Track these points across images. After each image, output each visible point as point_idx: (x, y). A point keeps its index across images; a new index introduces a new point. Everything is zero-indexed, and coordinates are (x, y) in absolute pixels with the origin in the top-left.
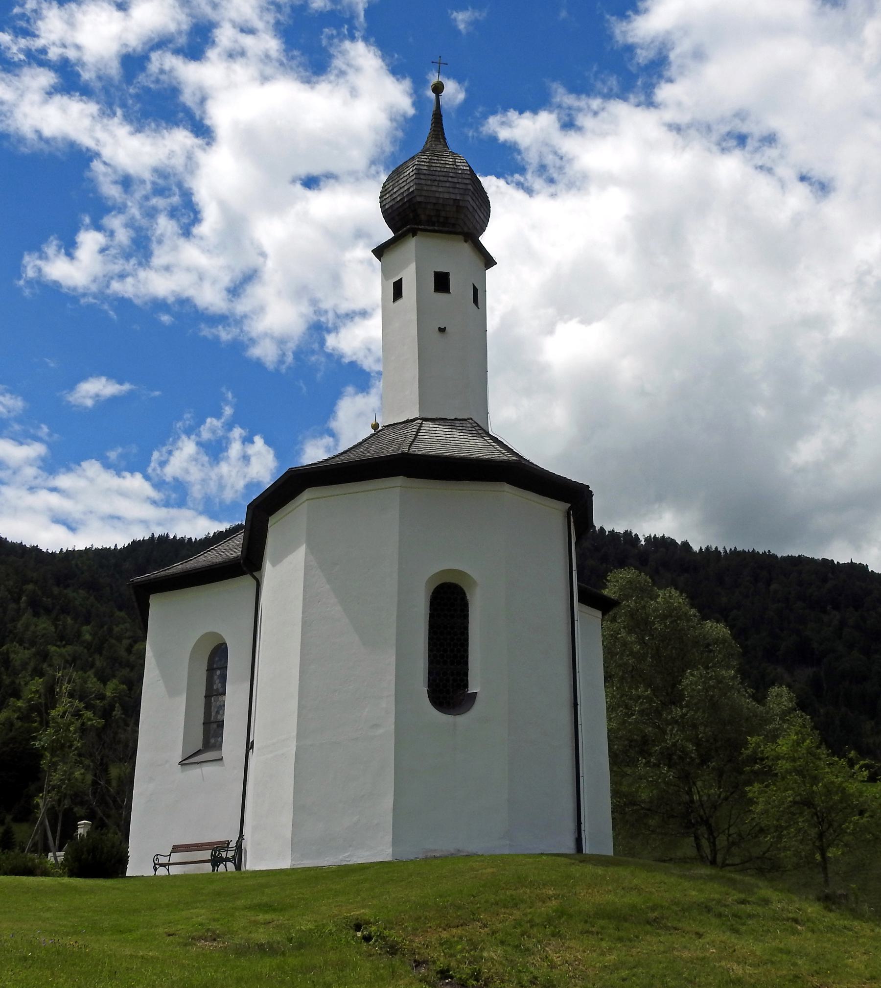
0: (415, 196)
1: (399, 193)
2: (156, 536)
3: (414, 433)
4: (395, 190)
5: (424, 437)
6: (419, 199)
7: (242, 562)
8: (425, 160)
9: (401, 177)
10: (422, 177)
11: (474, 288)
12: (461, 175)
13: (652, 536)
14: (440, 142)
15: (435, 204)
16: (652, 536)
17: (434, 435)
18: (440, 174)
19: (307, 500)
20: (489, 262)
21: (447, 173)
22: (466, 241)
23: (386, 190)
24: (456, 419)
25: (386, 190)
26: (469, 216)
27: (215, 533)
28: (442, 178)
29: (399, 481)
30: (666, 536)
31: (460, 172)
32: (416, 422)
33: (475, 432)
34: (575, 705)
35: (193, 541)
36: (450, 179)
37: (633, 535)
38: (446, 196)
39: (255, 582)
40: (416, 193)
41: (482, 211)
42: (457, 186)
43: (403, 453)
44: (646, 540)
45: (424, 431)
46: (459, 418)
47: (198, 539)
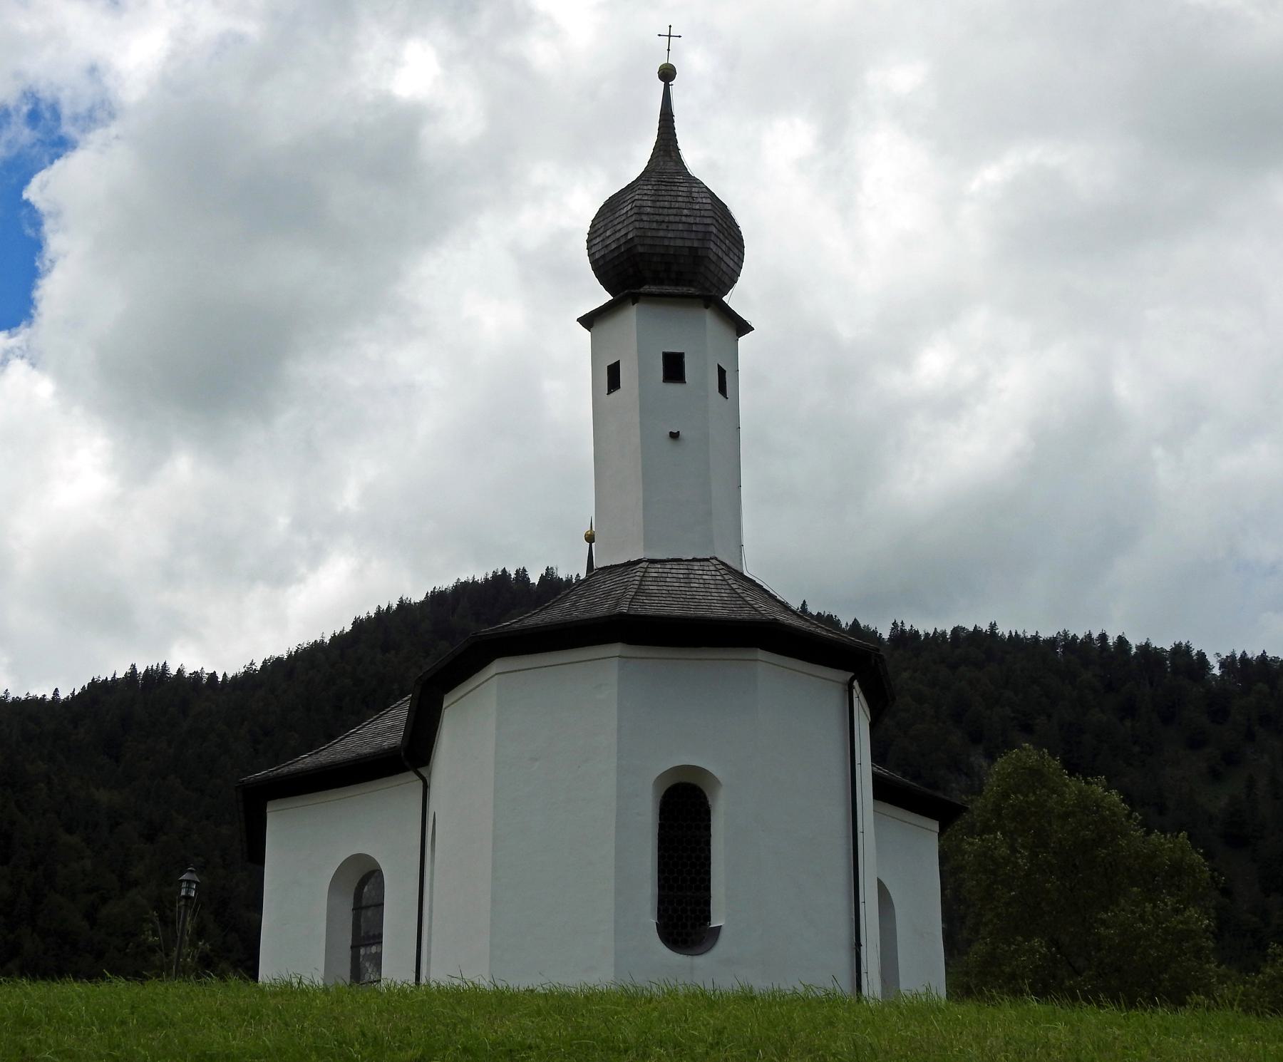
0: (636, 246)
1: (613, 238)
2: (141, 670)
3: (637, 582)
4: (608, 233)
5: (651, 587)
6: (640, 249)
7: (402, 754)
8: (649, 192)
9: (617, 215)
10: (645, 218)
11: (722, 373)
12: (698, 212)
13: (1238, 656)
14: (671, 156)
15: (663, 255)
16: (1238, 656)
17: (663, 584)
18: (671, 211)
19: (496, 674)
20: (742, 327)
21: (678, 211)
22: (707, 307)
23: (596, 231)
24: (695, 560)
25: (596, 231)
26: (712, 267)
27: (265, 662)
28: (672, 218)
29: (617, 649)
30: (1270, 654)
31: (697, 207)
32: (641, 565)
33: (719, 578)
34: (858, 944)
35: (220, 679)
36: (684, 219)
37: (1194, 652)
38: (679, 243)
39: (420, 783)
40: (636, 241)
41: (732, 257)
42: (694, 229)
43: (621, 615)
44: (1223, 664)
45: (650, 579)
46: (699, 557)
47: (230, 676)
